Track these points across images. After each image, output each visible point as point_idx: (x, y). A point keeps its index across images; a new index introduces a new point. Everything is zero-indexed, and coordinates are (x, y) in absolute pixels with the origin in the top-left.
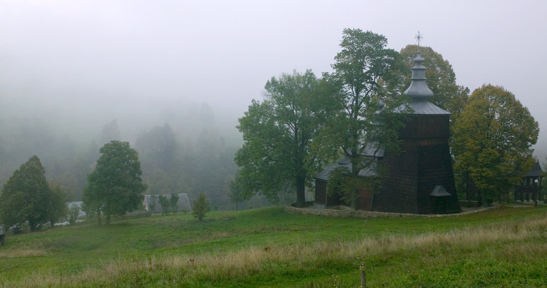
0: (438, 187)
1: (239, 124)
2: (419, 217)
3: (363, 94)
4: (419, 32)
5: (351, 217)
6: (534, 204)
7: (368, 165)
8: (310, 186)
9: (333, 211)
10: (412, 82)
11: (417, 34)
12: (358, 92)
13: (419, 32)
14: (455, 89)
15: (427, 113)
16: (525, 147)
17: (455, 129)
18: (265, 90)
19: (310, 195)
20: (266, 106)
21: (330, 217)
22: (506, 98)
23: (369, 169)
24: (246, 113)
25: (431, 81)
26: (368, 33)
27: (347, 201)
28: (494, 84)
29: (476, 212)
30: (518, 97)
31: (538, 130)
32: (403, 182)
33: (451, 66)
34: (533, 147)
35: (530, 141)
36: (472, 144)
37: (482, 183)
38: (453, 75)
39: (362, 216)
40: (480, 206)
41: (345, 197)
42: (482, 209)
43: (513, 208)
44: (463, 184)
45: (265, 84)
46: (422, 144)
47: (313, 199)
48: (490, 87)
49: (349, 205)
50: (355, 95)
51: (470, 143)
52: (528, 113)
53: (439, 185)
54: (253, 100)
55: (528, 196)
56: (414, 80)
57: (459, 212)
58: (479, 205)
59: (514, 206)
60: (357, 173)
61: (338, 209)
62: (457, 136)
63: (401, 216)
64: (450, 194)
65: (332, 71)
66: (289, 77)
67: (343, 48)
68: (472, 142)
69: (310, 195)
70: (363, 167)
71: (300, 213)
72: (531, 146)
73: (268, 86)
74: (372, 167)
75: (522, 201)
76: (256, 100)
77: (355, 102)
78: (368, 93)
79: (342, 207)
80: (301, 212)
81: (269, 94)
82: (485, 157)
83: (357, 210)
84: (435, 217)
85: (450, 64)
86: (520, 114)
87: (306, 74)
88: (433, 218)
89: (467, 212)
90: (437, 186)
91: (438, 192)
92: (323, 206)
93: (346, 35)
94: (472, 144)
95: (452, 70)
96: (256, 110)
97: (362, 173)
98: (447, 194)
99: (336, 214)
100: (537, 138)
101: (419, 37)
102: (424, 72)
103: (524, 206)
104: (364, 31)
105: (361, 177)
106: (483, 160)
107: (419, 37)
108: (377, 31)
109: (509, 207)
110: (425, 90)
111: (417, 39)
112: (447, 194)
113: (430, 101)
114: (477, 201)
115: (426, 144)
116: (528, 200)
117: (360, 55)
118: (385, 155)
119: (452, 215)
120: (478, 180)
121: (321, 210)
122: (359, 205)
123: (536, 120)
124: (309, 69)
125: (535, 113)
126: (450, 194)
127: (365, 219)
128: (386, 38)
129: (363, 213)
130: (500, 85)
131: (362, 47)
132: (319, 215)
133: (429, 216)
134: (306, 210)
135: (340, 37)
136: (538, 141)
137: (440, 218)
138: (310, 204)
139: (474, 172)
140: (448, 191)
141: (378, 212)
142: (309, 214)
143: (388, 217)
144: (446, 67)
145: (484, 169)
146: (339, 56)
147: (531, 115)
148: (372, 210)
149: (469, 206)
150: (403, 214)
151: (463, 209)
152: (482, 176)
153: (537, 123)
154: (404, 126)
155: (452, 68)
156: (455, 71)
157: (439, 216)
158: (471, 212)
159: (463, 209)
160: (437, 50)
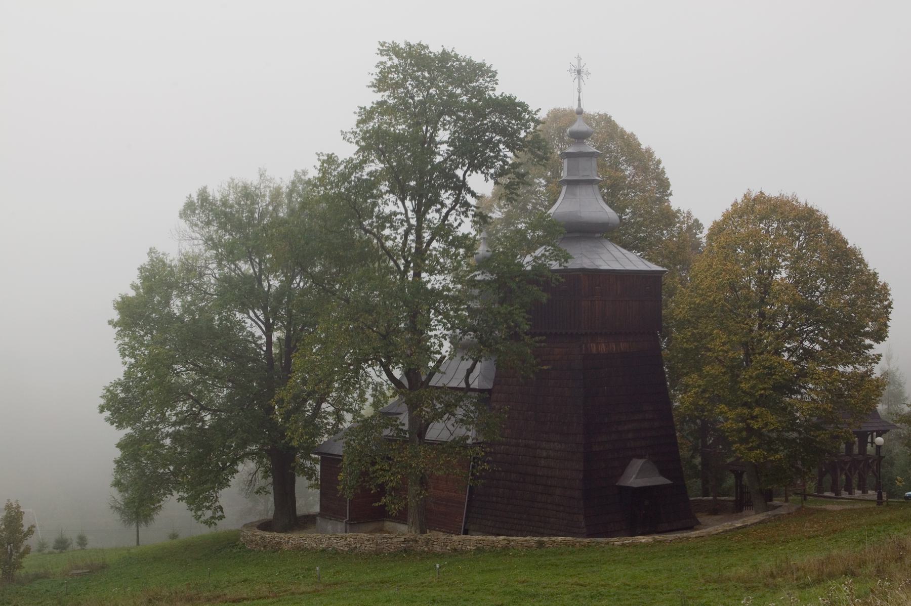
0: (637, 464)
1: (116, 316)
2: (589, 545)
3: (433, 216)
4: (579, 59)
5: (406, 552)
6: (876, 498)
7: (449, 408)
8: (310, 474)
9: (364, 539)
10: (564, 188)
11: (575, 63)
12: (420, 213)
13: (579, 59)
14: (669, 217)
15: (604, 267)
16: (857, 352)
17: (676, 307)
18: (184, 225)
19: (308, 498)
20: (190, 268)
21: (352, 555)
22: (809, 222)
23: (453, 419)
24: (135, 287)
25: (614, 193)
26: (445, 57)
27: (393, 509)
28: (772, 192)
29: (738, 524)
30: (836, 223)
31: (889, 306)
32: (545, 454)
33: (659, 162)
34: (878, 348)
35: (867, 335)
36: (724, 344)
37: (751, 449)
38: (664, 185)
39: (437, 548)
40: (741, 510)
41: (389, 498)
42: (752, 518)
43: (825, 510)
44: (693, 457)
45: (180, 205)
46: (594, 351)
47: (317, 509)
48: (761, 199)
49: (402, 518)
50: (413, 222)
51: (718, 342)
52: (861, 261)
53: (640, 457)
54: (152, 251)
55: (849, 480)
56: (569, 183)
57: (691, 528)
58: (740, 506)
59: (829, 507)
60: (421, 433)
61: (381, 530)
62: (681, 325)
63: (541, 545)
64: (668, 482)
65: (347, 151)
66: (245, 187)
67: (379, 97)
68: (724, 338)
69: (308, 498)
70: (438, 416)
71: (277, 547)
72: (871, 346)
73: (189, 209)
74: (460, 412)
75: (838, 493)
76: (160, 249)
77: (411, 237)
78: (447, 214)
79: (388, 525)
80: (279, 543)
81: (194, 235)
82: (758, 377)
83: (423, 532)
84: (634, 545)
85: (657, 156)
86: (843, 262)
87: (293, 183)
88: (630, 545)
89: (715, 526)
90: (634, 460)
91: (637, 476)
92: (340, 526)
93: (385, 59)
94: (724, 344)
95: (663, 172)
96: (157, 279)
97: (437, 431)
98: (661, 480)
99: (369, 547)
100: (886, 326)
101: (579, 72)
102: (594, 162)
103: (858, 506)
104: (435, 49)
105: (431, 443)
106: (753, 387)
107: (579, 72)
108: (468, 49)
109: (817, 510)
110: (593, 207)
111: (574, 75)
112: (661, 480)
113: (613, 240)
114: (733, 498)
115: (603, 348)
116: (849, 490)
117: (425, 116)
118: (498, 380)
119: (678, 535)
120: (743, 441)
121: (335, 535)
122: (432, 518)
123: (881, 279)
124: (299, 170)
125: (879, 259)
126: (668, 482)
127: (440, 556)
128: (493, 69)
129: (439, 539)
130: (788, 193)
131: (437, 115)
132: (323, 550)
133: (617, 541)
134: (295, 537)
135: (369, 64)
136: (891, 331)
137: (647, 545)
138: (308, 521)
139: (728, 418)
140: (663, 473)
141: (480, 537)
142: (298, 548)
143: (506, 548)
144: (644, 161)
145: (757, 411)
146: (367, 115)
147: (871, 267)
148: (466, 532)
149: (716, 510)
150: (546, 539)
151: (702, 518)
152: (749, 429)
153: (885, 286)
154: (544, 297)
155: (661, 166)
156: (668, 174)
157: (643, 539)
158: (727, 525)
159: (702, 518)
160: (626, 122)
